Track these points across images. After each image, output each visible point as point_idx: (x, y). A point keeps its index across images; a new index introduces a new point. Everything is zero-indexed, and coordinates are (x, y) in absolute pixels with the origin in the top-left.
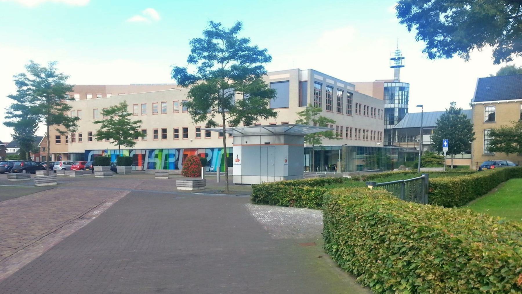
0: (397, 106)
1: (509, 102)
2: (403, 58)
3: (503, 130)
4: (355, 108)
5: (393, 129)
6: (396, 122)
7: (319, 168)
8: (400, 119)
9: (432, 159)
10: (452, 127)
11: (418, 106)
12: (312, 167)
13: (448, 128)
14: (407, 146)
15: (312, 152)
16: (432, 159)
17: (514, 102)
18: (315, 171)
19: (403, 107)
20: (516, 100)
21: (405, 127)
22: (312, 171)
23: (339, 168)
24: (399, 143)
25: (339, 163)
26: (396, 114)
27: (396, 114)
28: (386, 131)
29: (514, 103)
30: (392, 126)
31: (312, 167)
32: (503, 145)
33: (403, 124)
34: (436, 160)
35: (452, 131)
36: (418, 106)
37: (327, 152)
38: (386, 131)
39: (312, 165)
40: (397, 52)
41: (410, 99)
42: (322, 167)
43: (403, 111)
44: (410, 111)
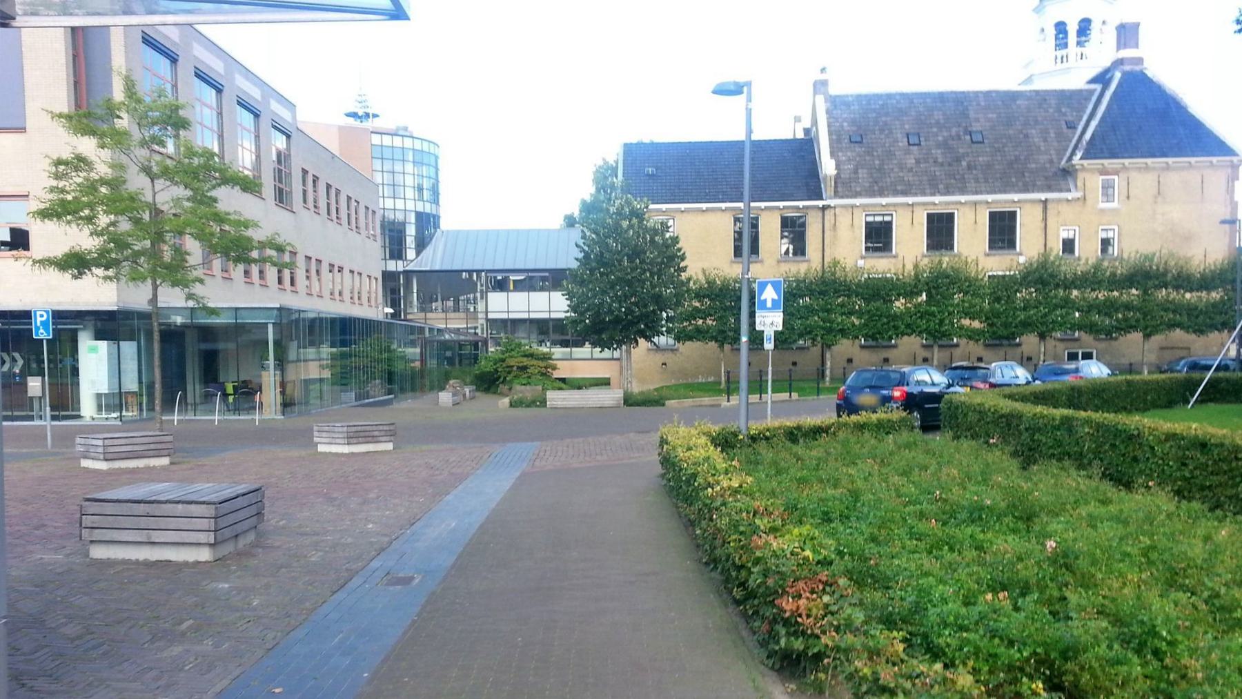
0: (410, 206)
1: (707, 210)
2: (375, 116)
3: (711, 283)
4: (301, 187)
5: (405, 272)
6: (411, 254)
7: (184, 398)
8: (421, 245)
9: (526, 362)
10: (631, 260)
11: (721, 91)
12: (151, 395)
13: (620, 261)
14: (446, 322)
15: (149, 334)
16: (526, 362)
17: (721, 210)
18: (168, 405)
19: (428, 210)
20: (723, 205)
21: (437, 268)
22: (151, 408)
23: (270, 396)
24: (422, 315)
25: (270, 379)
26: (411, 231)
27: (411, 231)
28: (388, 277)
29: (719, 214)
30: (400, 263)
31: (151, 395)
32: (709, 322)
33: (433, 259)
34: (535, 362)
35: (633, 270)
36: (721, 91)
37: (207, 333)
38: (388, 277)
39: (151, 387)
40: (360, 99)
41: (442, 188)
42: (194, 388)
43: (428, 223)
44: (445, 224)
